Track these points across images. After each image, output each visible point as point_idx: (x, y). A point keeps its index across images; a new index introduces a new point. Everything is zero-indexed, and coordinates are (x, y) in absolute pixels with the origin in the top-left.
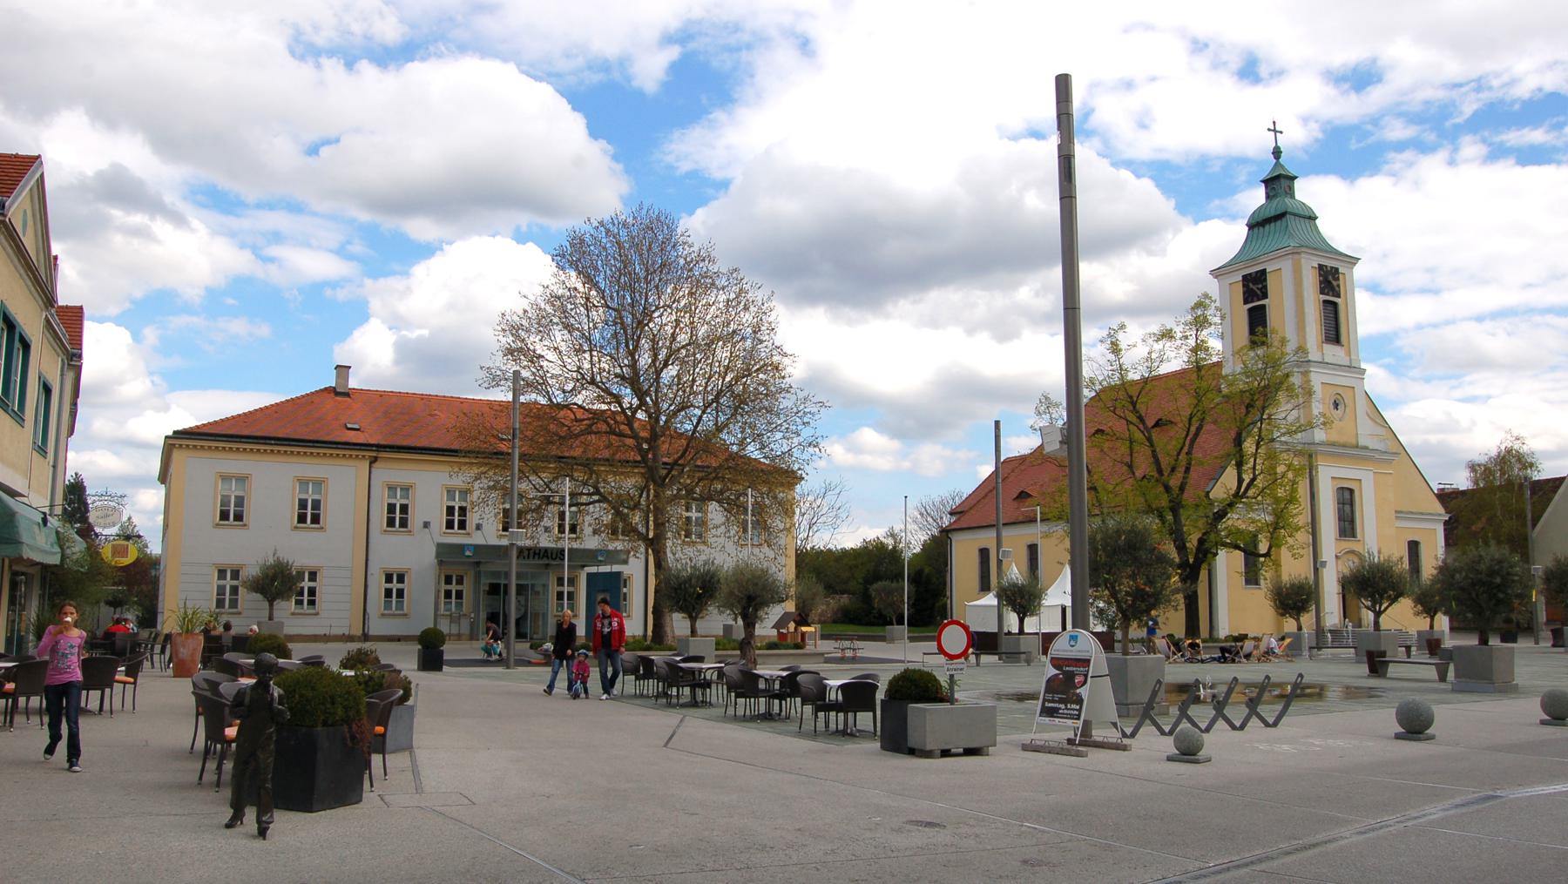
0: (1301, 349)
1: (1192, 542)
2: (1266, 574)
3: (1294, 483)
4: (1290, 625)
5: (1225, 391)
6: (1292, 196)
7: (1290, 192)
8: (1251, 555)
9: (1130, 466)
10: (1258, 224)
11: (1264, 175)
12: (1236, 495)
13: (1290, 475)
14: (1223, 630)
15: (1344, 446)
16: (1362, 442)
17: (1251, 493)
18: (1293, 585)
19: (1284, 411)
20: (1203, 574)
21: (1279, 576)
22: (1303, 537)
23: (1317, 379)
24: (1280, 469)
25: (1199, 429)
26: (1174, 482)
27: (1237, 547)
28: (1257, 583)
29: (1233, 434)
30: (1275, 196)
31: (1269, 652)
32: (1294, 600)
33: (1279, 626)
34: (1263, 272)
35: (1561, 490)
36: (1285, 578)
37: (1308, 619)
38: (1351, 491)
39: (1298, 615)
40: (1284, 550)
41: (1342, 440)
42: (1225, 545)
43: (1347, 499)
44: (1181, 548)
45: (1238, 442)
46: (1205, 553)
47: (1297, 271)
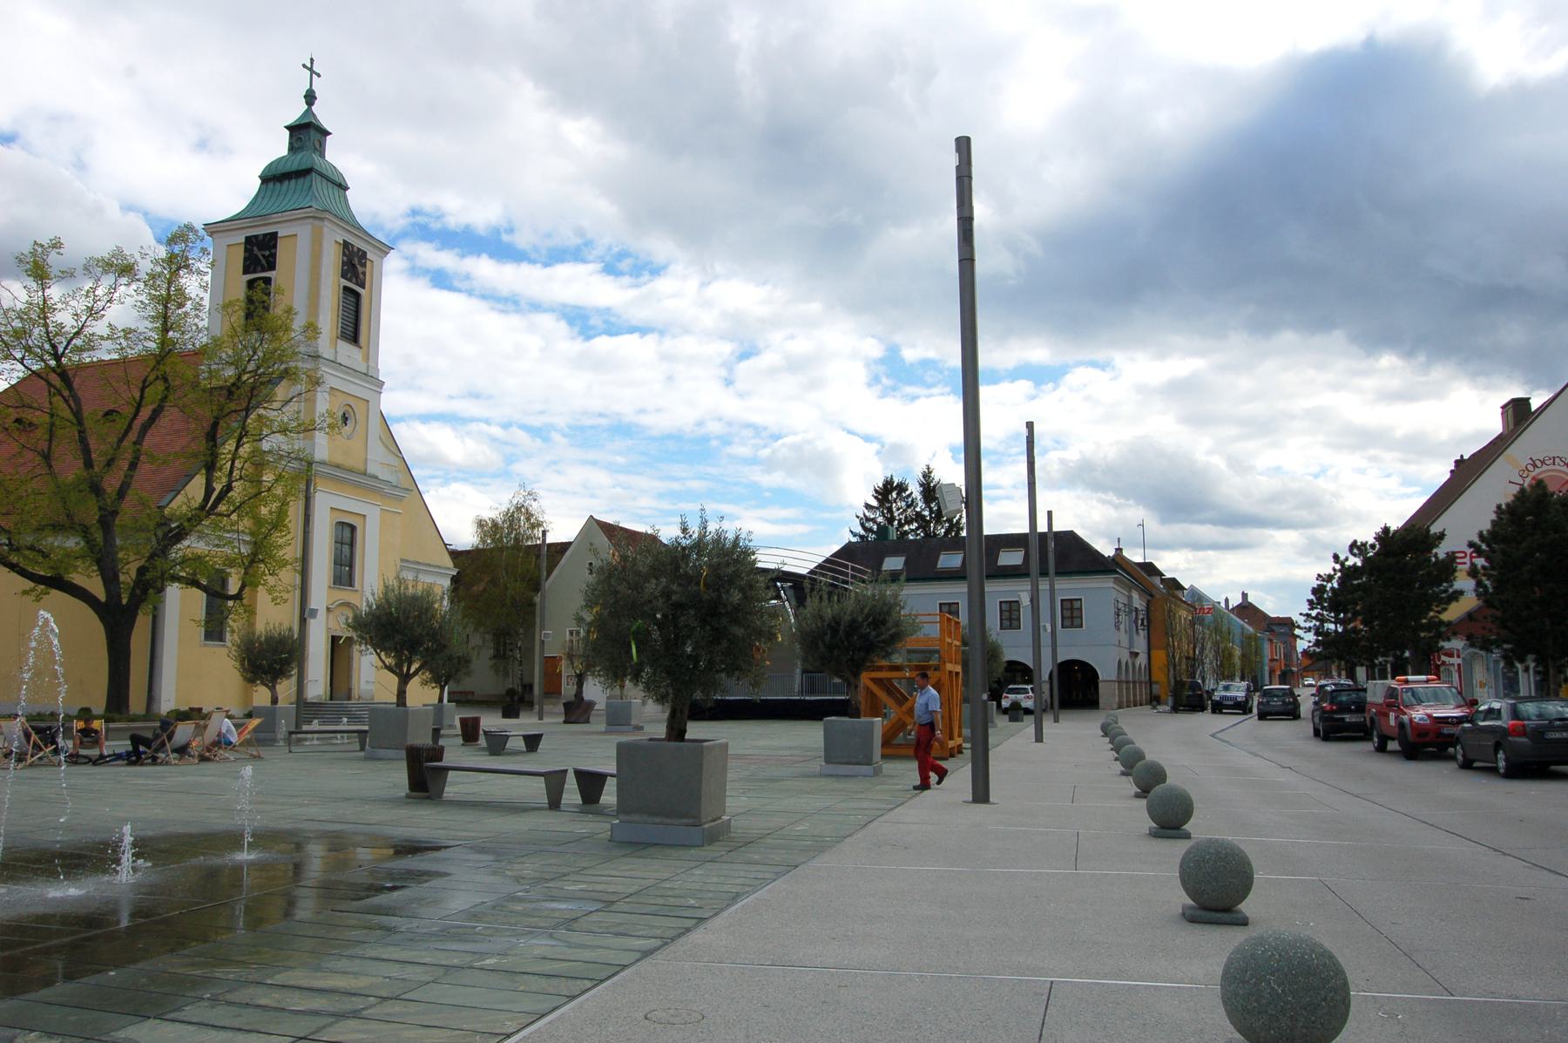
0: (312, 329)
1: (128, 576)
2: (235, 624)
3: (285, 504)
4: (261, 696)
5: (205, 384)
6: (322, 155)
7: (321, 149)
8: (216, 595)
9: (47, 457)
10: (273, 178)
11: (290, 122)
12: (202, 507)
13: (279, 491)
14: (168, 702)
15: (350, 471)
16: (371, 470)
17: (222, 508)
18: (269, 639)
19: (280, 407)
20: (142, 622)
21: (251, 624)
22: (289, 576)
23: (332, 378)
24: (268, 477)
25: (156, 414)
26: (111, 484)
27: (194, 583)
28: (221, 638)
29: (207, 425)
30: (301, 148)
31: (221, 742)
32: (270, 660)
33: (247, 697)
34: (274, 236)
35: (568, 553)
36: (260, 628)
37: (286, 688)
38: (353, 528)
39: (274, 680)
40: (261, 592)
41: (349, 463)
42: (175, 578)
43: (347, 536)
44: (110, 579)
45: (212, 437)
46: (148, 587)
47: (317, 242)
